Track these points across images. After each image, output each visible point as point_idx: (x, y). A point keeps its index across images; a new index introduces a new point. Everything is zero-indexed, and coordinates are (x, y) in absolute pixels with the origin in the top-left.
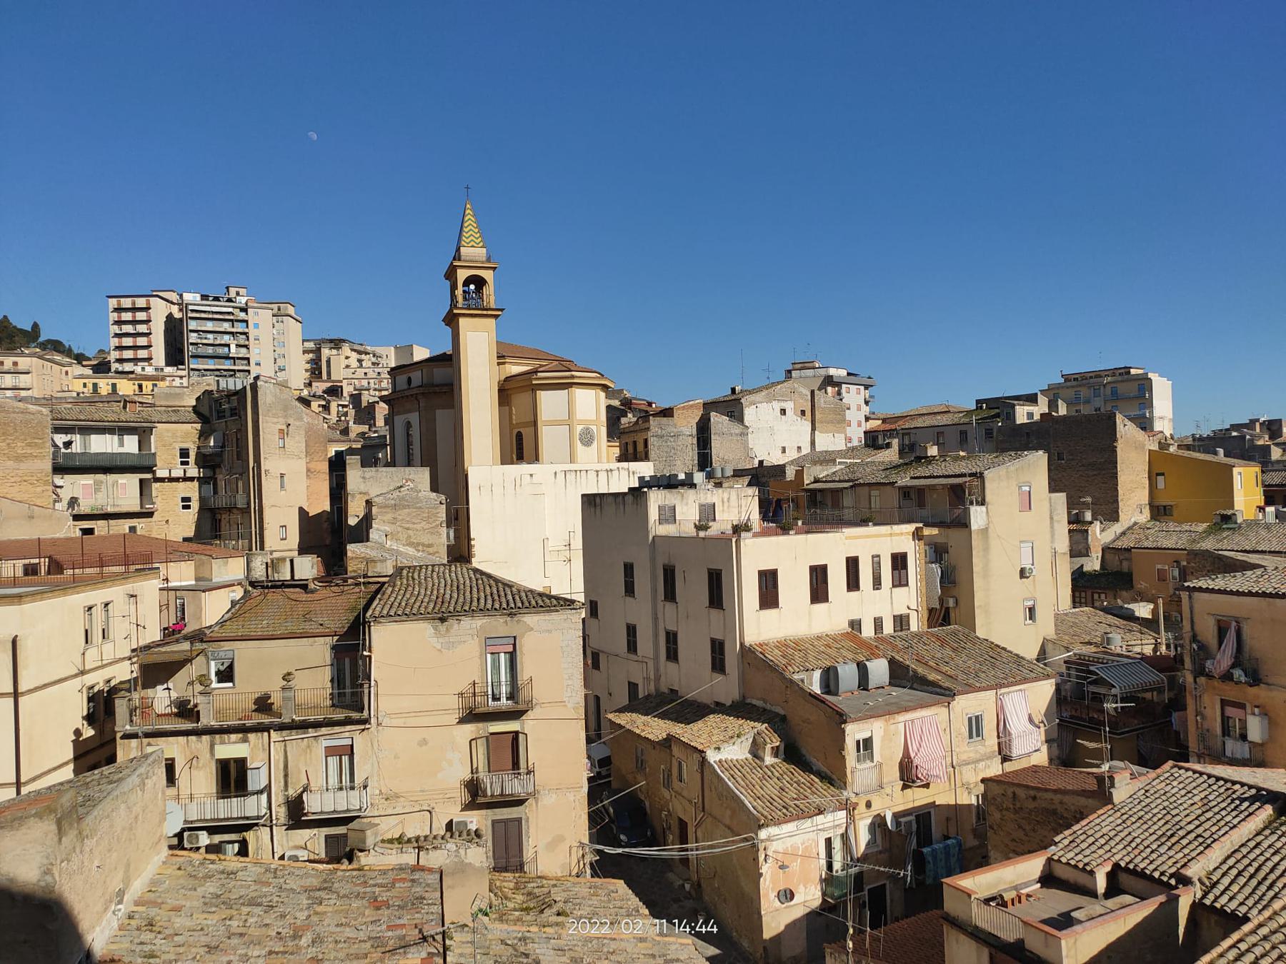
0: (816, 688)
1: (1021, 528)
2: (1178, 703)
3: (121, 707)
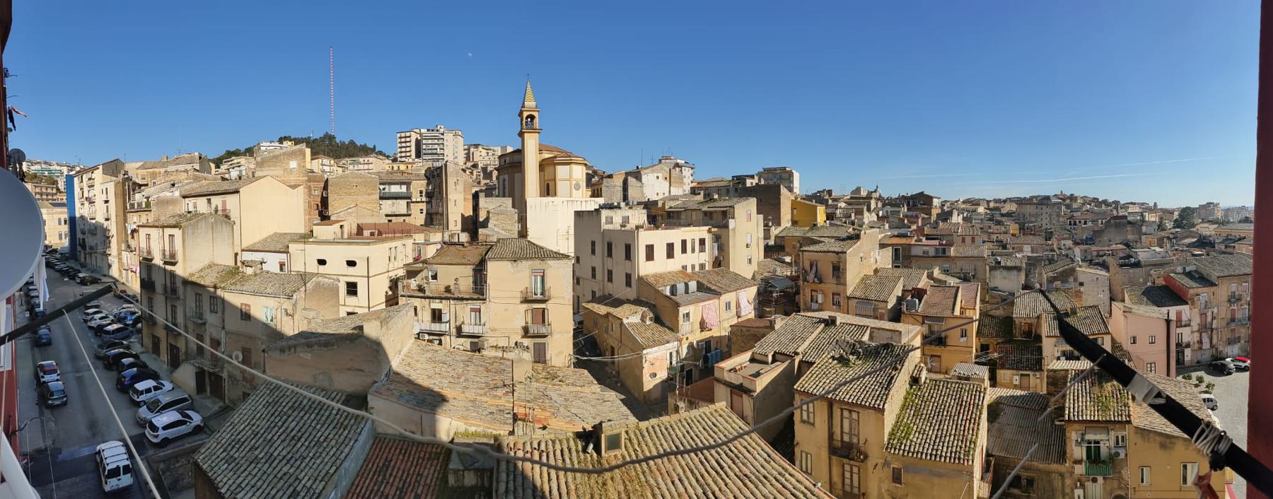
0: (668, 293)
1: (747, 224)
2: (798, 293)
3: (400, 285)
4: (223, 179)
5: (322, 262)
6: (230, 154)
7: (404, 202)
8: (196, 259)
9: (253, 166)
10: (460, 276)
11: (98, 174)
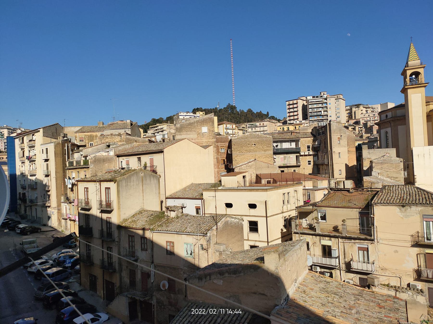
4: (150, 141)
5: (229, 205)
6: (155, 122)
7: (293, 156)
8: (128, 208)
9: (173, 131)
10: (350, 219)
11: (39, 137)
